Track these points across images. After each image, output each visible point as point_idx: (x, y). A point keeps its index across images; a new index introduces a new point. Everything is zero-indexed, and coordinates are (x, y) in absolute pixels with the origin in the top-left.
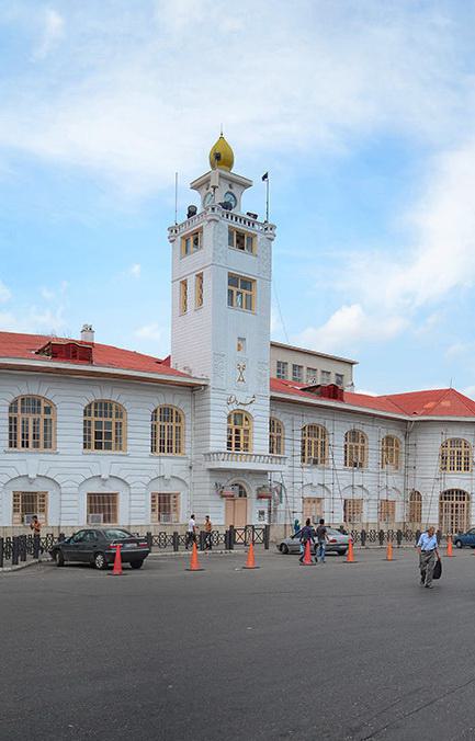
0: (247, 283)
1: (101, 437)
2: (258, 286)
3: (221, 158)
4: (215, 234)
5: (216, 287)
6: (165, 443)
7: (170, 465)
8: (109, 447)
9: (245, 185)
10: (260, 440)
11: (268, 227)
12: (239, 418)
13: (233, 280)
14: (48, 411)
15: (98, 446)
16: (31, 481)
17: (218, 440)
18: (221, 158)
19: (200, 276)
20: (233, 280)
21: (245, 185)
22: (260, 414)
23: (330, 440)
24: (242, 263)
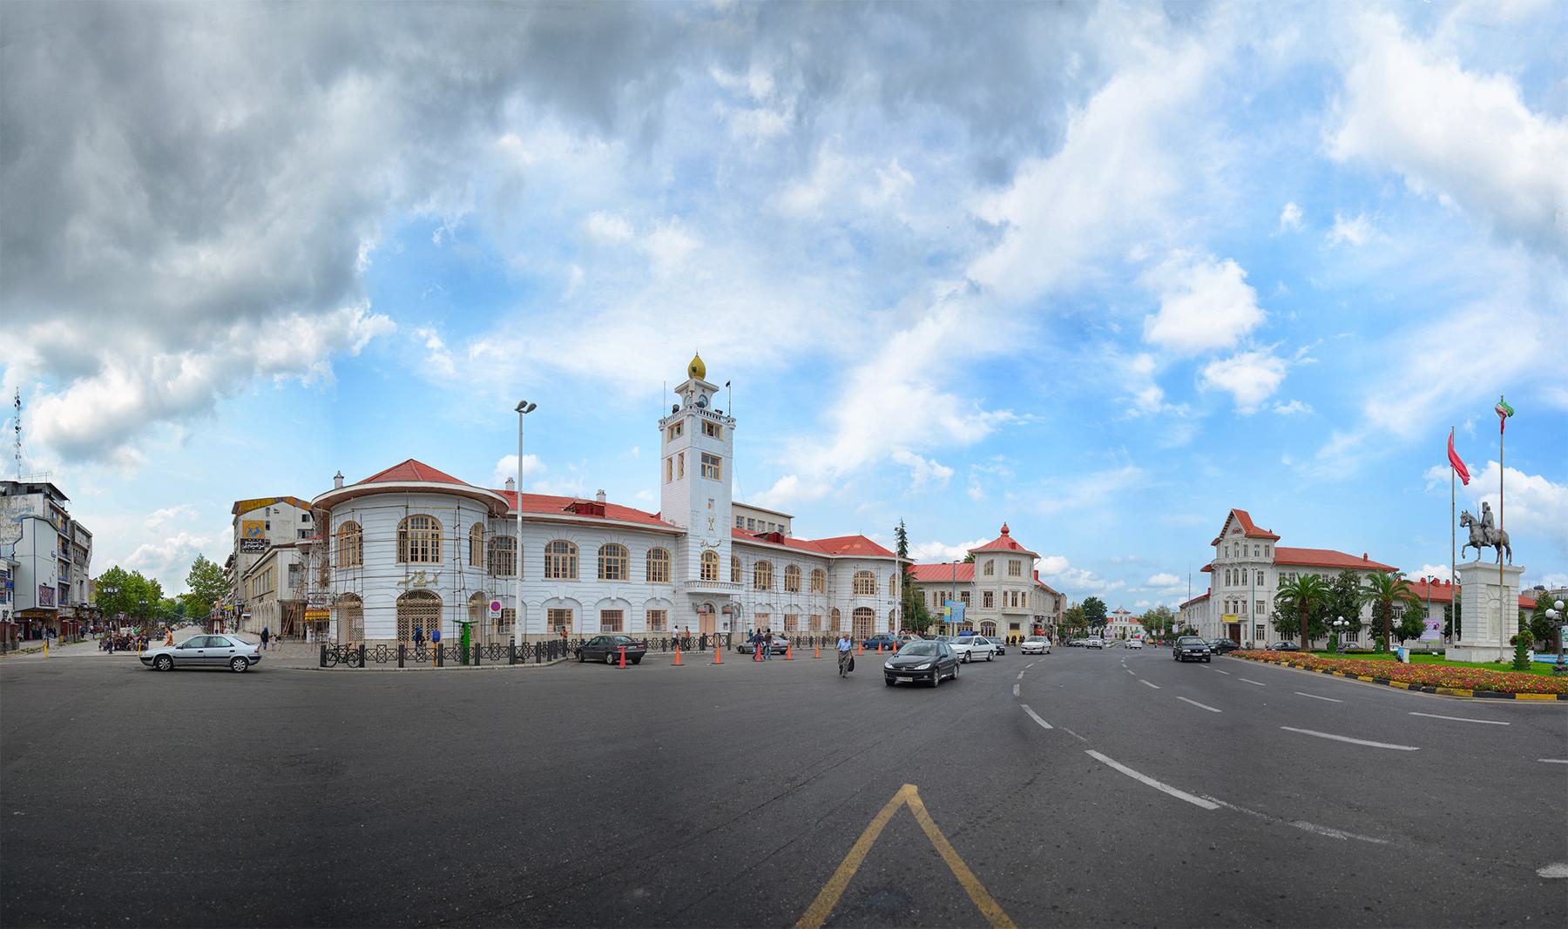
0: (715, 460)
1: (611, 569)
2: (723, 463)
3: (696, 371)
4: (692, 426)
5: (693, 463)
6: (656, 574)
7: (660, 590)
8: (616, 577)
9: (714, 390)
10: (724, 572)
11: (730, 420)
12: (709, 556)
13: (705, 457)
14: (573, 551)
15: (609, 577)
16: (561, 602)
17: (694, 572)
18: (696, 371)
19: (682, 455)
20: (705, 457)
21: (714, 390)
22: (725, 554)
24: (712, 446)
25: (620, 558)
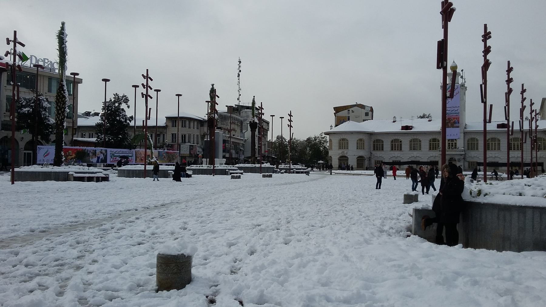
23: (422, 143)
25: (437, 143)
